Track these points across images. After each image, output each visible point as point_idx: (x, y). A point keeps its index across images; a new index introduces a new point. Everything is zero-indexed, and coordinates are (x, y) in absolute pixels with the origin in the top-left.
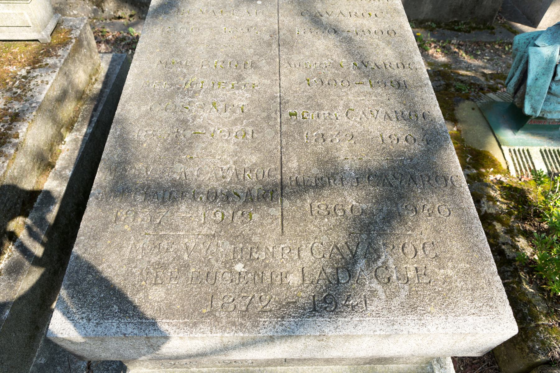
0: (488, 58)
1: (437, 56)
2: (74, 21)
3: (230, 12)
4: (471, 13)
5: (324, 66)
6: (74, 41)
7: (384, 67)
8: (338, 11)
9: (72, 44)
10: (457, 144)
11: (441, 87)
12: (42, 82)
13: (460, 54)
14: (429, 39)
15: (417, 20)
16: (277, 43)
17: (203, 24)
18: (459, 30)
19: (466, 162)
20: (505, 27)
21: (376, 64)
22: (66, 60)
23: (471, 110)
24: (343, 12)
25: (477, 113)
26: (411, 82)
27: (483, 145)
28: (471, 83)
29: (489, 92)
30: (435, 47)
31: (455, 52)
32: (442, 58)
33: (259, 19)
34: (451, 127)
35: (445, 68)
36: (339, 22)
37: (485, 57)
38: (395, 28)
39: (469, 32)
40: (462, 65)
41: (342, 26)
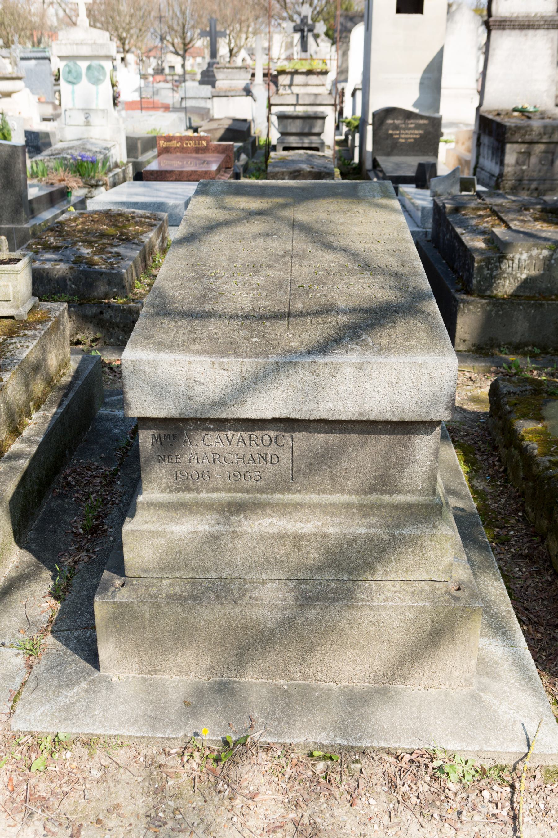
6: (54, 319)
12: (22, 346)
15: (510, 344)
22: (45, 333)
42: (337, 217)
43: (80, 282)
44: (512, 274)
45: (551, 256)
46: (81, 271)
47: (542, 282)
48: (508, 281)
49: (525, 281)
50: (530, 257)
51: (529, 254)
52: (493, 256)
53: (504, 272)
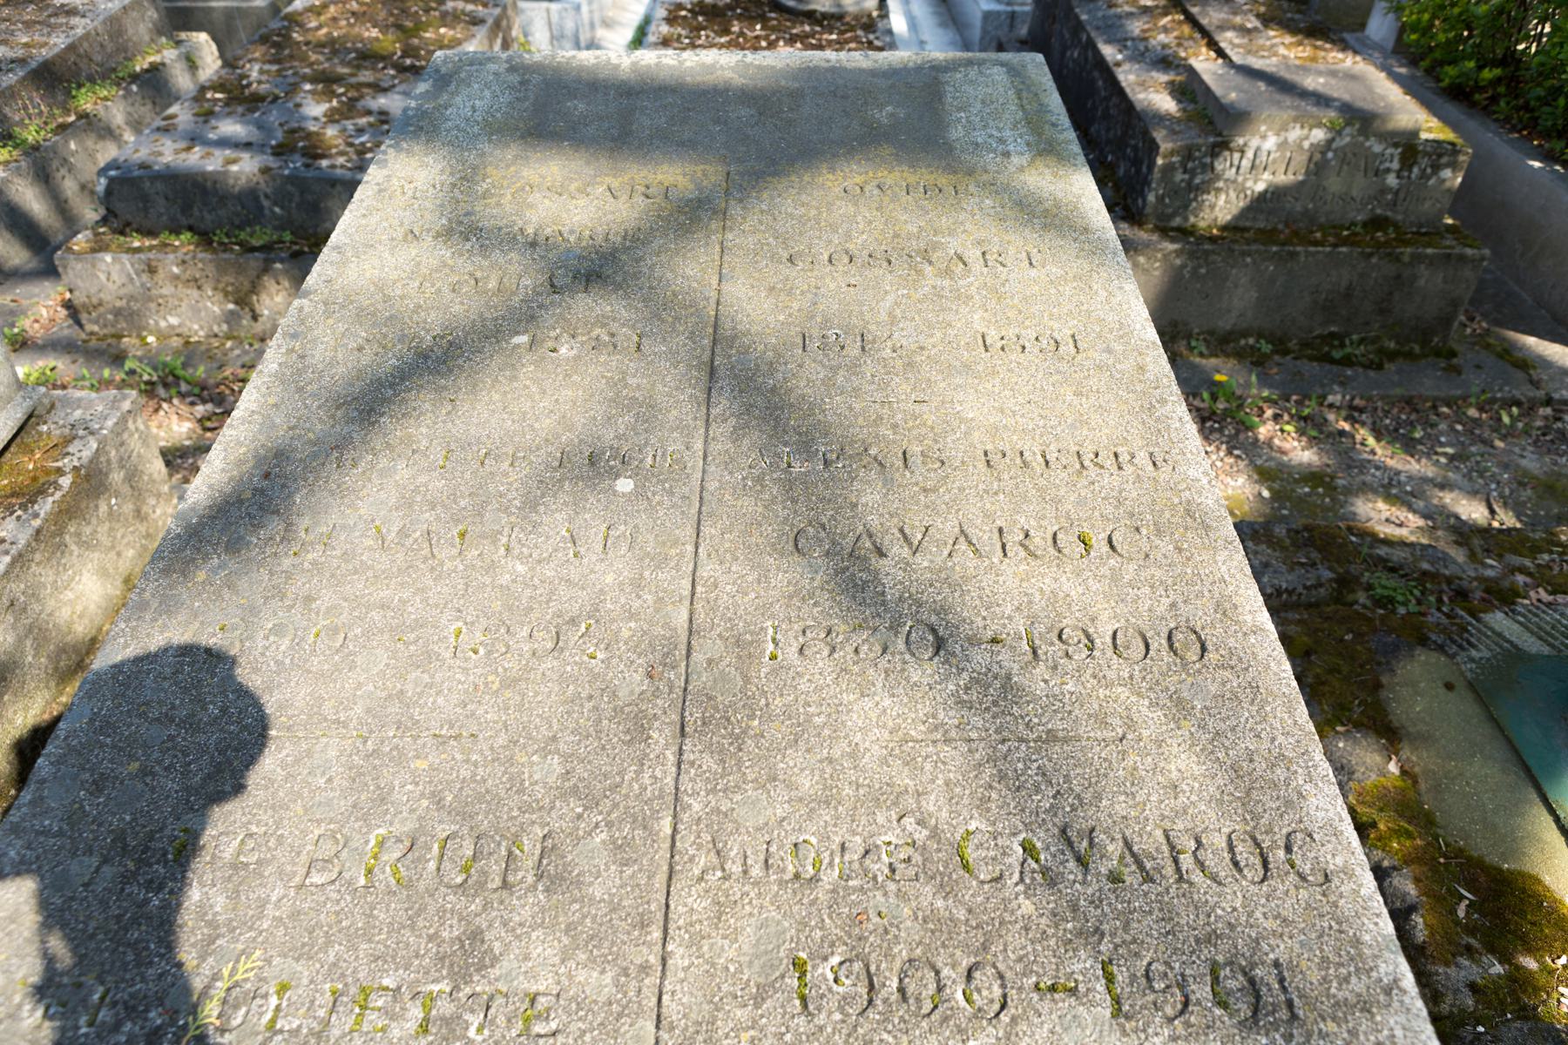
0: (1450, 450)
1: (1286, 446)
2: (90, 404)
3: (494, 537)
4: (1382, 312)
5: (880, 868)
6: (66, 481)
7: (1169, 870)
8: (950, 527)
9: (58, 495)
10: (1409, 835)
11: (1322, 590)
13: (1358, 438)
14: (1254, 391)
15: (1211, 333)
16: (675, 717)
17: (369, 608)
18: (1347, 361)
19: (1457, 923)
20: (1488, 346)
21: (1128, 845)
23: (1442, 690)
24: (970, 531)
25: (1461, 705)
26: (1315, 976)
27: (1513, 843)
28: (1425, 573)
29: (1488, 606)
30: (1276, 417)
31: (1342, 433)
32: (1300, 453)
33: (611, 573)
34: (1378, 758)
35: (1313, 488)
36: (954, 586)
37: (1440, 450)
38: (1200, 613)
39: (1380, 367)
40: (1368, 478)
41: (972, 613)
42: (884, 300)
43: (290, 201)
44: (1234, 181)
45: (1330, 142)
46: (288, 177)
47: (1296, 199)
48: (1223, 197)
49: (1262, 198)
50: (1282, 145)
51: (1282, 139)
52: (1200, 141)
53: (1218, 177)
